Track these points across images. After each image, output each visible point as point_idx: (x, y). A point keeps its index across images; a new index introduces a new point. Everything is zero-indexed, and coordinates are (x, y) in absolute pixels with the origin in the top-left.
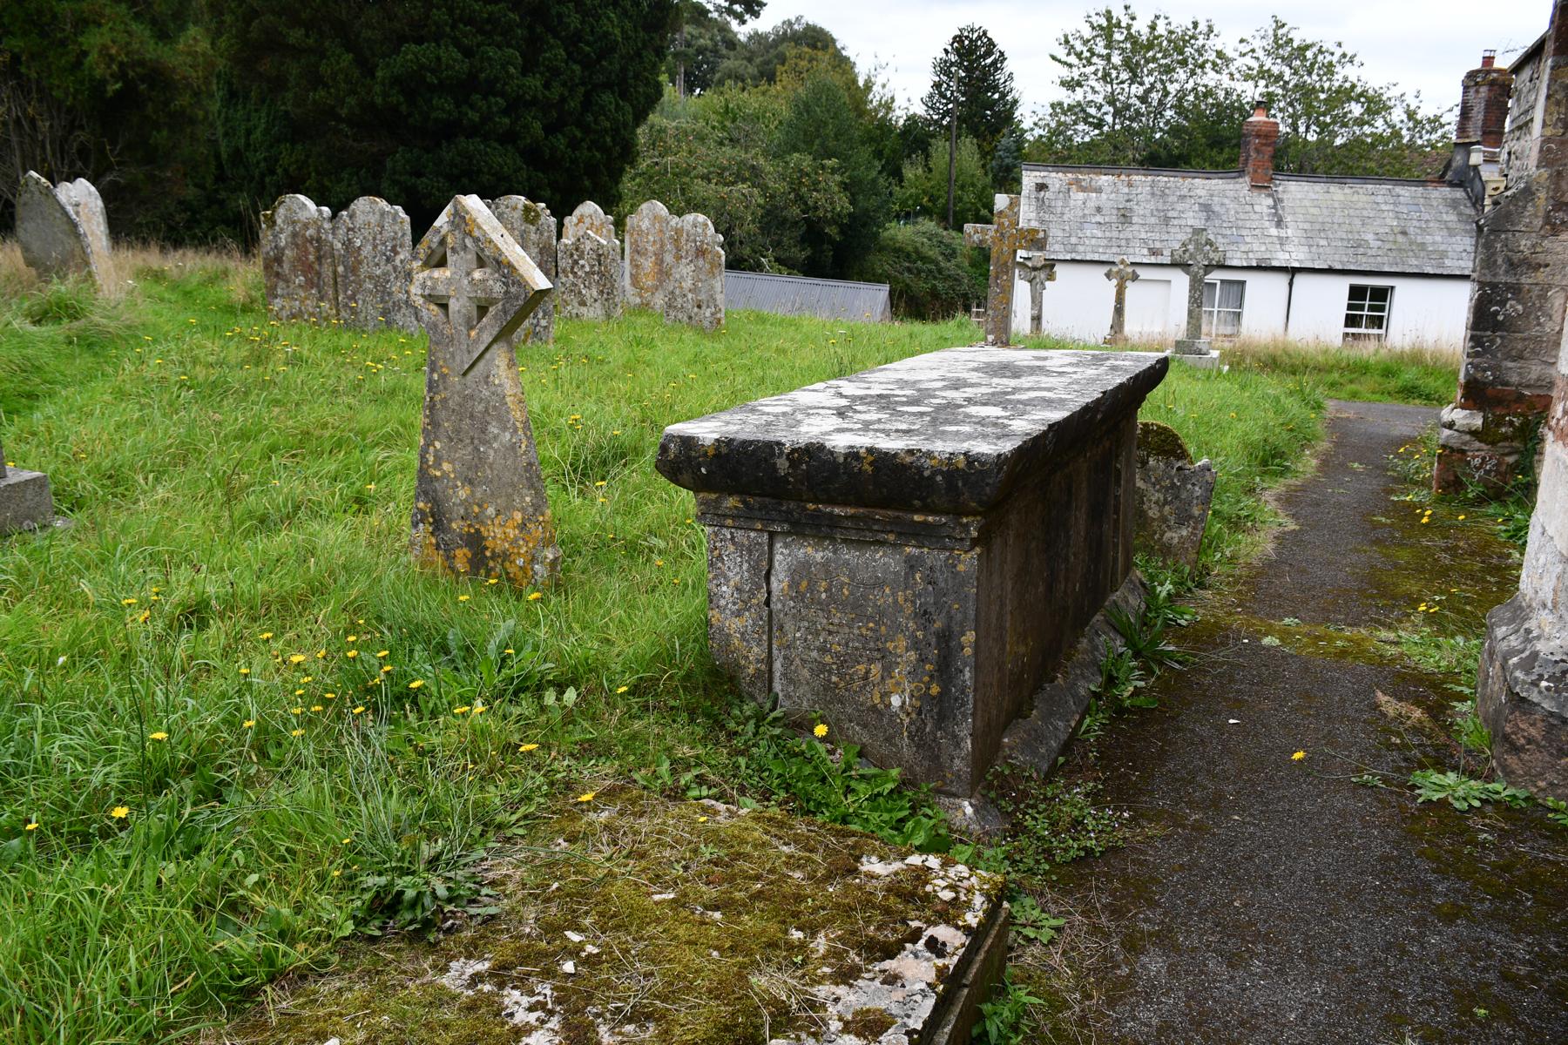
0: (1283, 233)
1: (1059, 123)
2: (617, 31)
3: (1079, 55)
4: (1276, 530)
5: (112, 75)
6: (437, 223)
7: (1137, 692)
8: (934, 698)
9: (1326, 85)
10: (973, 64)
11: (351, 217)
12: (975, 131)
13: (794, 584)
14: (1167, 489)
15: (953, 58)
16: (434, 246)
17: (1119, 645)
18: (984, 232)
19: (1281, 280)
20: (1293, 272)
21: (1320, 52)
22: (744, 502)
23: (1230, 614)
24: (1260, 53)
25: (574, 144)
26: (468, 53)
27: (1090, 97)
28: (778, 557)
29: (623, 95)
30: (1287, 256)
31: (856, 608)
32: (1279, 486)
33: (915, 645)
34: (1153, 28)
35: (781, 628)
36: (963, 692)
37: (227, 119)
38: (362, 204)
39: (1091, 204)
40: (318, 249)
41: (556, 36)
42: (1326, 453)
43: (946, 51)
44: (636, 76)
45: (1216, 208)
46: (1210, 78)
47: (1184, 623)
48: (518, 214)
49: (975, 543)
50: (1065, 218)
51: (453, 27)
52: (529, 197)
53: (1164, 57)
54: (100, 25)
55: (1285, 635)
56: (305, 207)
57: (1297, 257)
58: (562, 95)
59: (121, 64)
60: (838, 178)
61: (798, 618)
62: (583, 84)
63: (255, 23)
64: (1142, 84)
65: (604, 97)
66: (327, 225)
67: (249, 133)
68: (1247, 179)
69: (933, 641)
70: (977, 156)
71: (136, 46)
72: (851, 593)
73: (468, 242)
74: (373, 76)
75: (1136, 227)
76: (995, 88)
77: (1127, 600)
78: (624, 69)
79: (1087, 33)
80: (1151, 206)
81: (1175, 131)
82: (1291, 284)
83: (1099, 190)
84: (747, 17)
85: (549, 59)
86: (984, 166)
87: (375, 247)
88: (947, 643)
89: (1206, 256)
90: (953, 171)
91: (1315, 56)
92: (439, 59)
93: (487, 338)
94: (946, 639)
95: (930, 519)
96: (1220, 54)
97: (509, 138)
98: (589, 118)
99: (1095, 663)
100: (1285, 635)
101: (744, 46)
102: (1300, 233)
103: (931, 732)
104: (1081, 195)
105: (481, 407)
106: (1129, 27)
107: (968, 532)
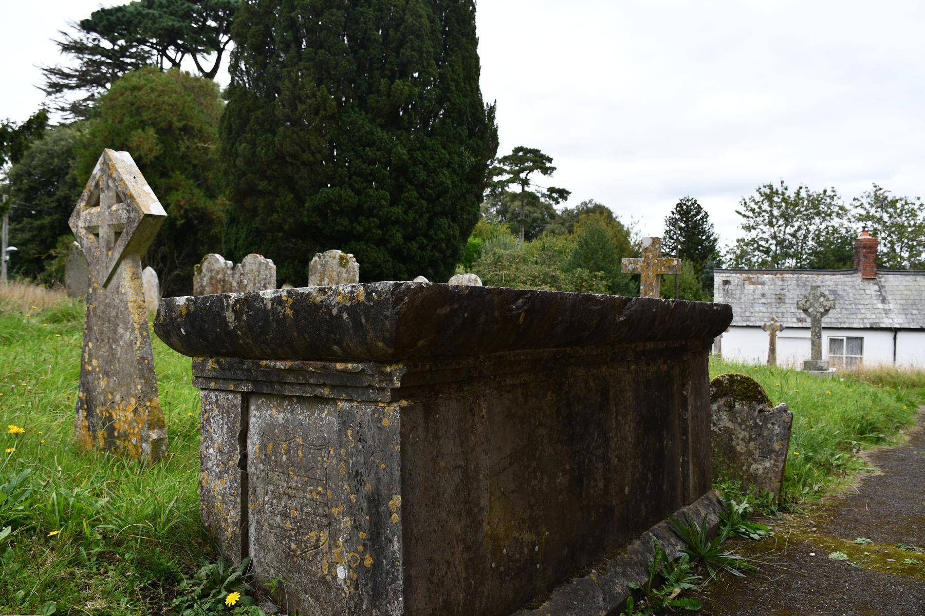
0: (886, 307)
1: (742, 251)
2: (449, 182)
3: (753, 210)
4: (864, 475)
5: (180, 216)
6: (94, 172)
7: (684, 593)
8: (368, 571)
9: (912, 223)
10: (689, 222)
11: (243, 266)
12: (691, 257)
13: (263, 447)
14: (751, 428)
15: (677, 216)
16: (92, 189)
17: (679, 550)
18: (635, 263)
19: (889, 336)
20: (895, 331)
21: (906, 203)
22: (218, 362)
23: (805, 532)
24: (867, 206)
25: (422, 247)
26: (358, 192)
27: (761, 235)
28: (252, 420)
29: (454, 220)
30: (891, 321)
31: (306, 469)
32: (874, 448)
33: (350, 510)
34: (798, 194)
35: (254, 492)
36: (393, 566)
37: (227, 234)
38: (249, 259)
39: (758, 292)
40: (223, 286)
41: (411, 183)
42: (918, 433)
43: (673, 213)
44: (462, 209)
45: (841, 293)
46: (836, 222)
47: (756, 537)
48: (336, 261)
49: (397, 395)
50: (742, 301)
51: (350, 178)
52: (343, 251)
53: (806, 210)
54: (177, 190)
55: (854, 552)
56: (219, 261)
57: (897, 321)
58: (414, 218)
59: (186, 210)
60: (604, 282)
61: (267, 481)
62: (428, 212)
63: (243, 180)
64: (793, 226)
65: (441, 220)
66: (229, 272)
67: (237, 240)
68: (860, 274)
69: (365, 505)
70: (693, 272)
71: (194, 200)
72: (305, 456)
73: (110, 182)
74: (303, 206)
75: (788, 305)
76: (704, 232)
77: (700, 514)
78: (454, 204)
79: (758, 198)
80: (797, 292)
81: (815, 253)
82: (895, 339)
83: (763, 284)
84: (560, 200)
85: (407, 197)
86: (697, 278)
87: (255, 284)
88: (377, 507)
89: (821, 304)
90: (678, 281)
91: (903, 206)
92: (340, 196)
93: (117, 256)
94: (376, 501)
95: (350, 366)
96: (842, 208)
97: (382, 242)
98: (432, 232)
99: (644, 564)
100: (854, 552)
101: (560, 217)
102: (898, 306)
103: (368, 610)
104: (752, 287)
105: (114, 313)
106: (783, 194)
107: (392, 381)
